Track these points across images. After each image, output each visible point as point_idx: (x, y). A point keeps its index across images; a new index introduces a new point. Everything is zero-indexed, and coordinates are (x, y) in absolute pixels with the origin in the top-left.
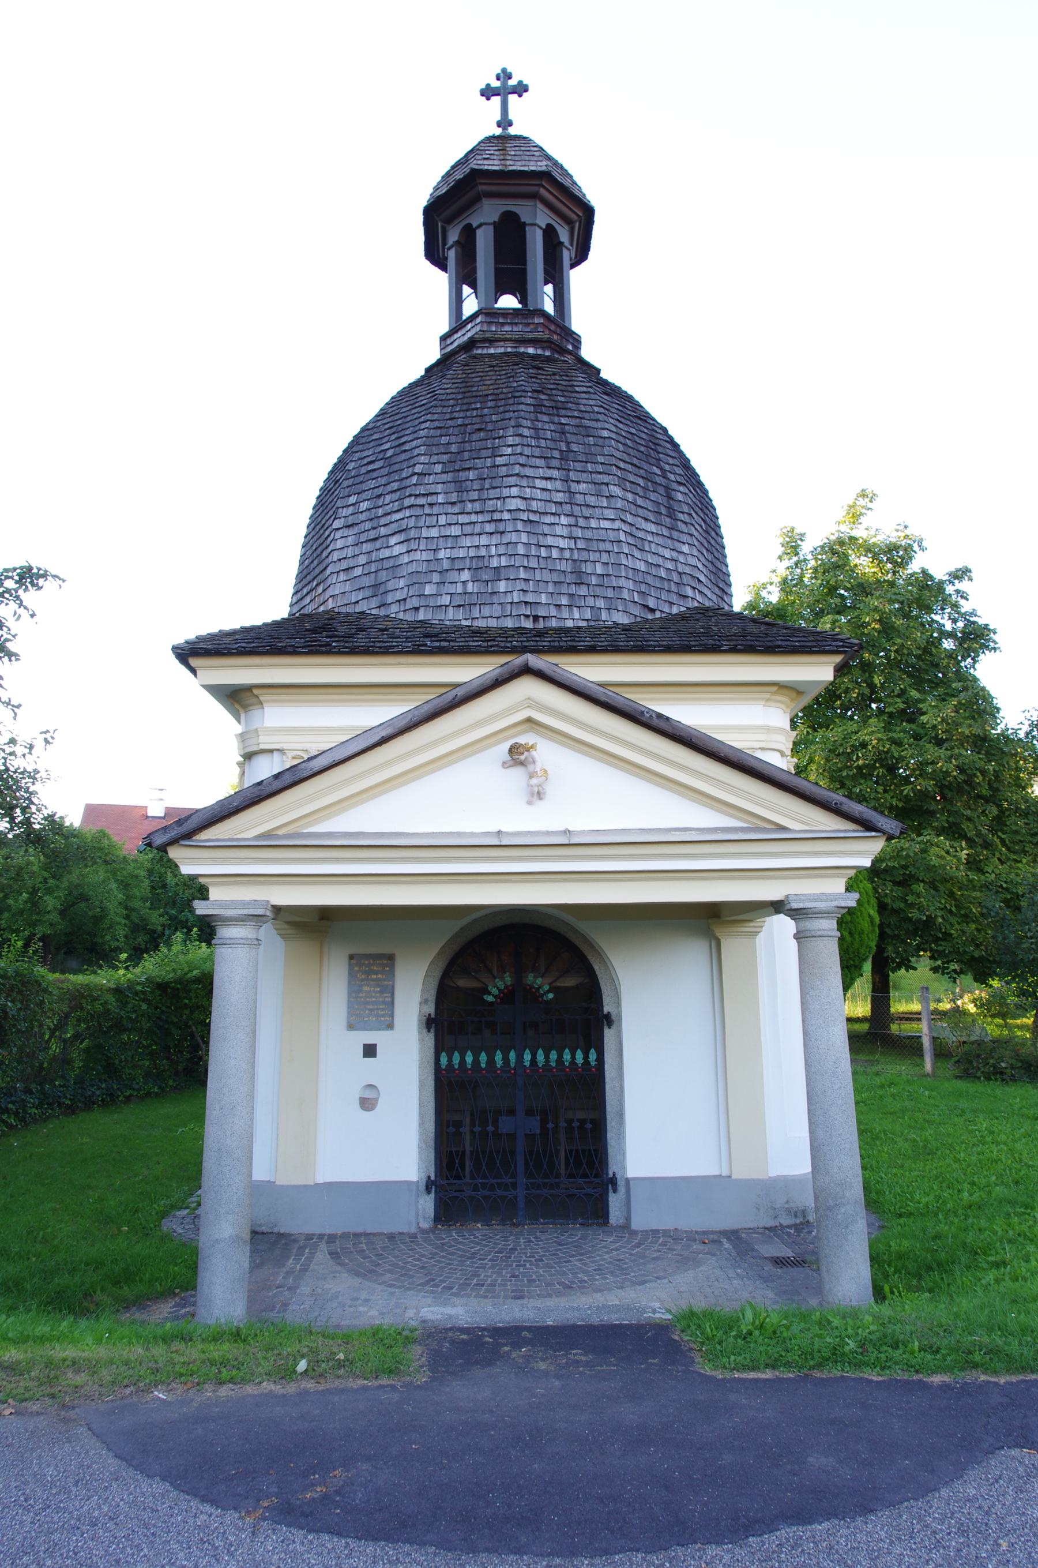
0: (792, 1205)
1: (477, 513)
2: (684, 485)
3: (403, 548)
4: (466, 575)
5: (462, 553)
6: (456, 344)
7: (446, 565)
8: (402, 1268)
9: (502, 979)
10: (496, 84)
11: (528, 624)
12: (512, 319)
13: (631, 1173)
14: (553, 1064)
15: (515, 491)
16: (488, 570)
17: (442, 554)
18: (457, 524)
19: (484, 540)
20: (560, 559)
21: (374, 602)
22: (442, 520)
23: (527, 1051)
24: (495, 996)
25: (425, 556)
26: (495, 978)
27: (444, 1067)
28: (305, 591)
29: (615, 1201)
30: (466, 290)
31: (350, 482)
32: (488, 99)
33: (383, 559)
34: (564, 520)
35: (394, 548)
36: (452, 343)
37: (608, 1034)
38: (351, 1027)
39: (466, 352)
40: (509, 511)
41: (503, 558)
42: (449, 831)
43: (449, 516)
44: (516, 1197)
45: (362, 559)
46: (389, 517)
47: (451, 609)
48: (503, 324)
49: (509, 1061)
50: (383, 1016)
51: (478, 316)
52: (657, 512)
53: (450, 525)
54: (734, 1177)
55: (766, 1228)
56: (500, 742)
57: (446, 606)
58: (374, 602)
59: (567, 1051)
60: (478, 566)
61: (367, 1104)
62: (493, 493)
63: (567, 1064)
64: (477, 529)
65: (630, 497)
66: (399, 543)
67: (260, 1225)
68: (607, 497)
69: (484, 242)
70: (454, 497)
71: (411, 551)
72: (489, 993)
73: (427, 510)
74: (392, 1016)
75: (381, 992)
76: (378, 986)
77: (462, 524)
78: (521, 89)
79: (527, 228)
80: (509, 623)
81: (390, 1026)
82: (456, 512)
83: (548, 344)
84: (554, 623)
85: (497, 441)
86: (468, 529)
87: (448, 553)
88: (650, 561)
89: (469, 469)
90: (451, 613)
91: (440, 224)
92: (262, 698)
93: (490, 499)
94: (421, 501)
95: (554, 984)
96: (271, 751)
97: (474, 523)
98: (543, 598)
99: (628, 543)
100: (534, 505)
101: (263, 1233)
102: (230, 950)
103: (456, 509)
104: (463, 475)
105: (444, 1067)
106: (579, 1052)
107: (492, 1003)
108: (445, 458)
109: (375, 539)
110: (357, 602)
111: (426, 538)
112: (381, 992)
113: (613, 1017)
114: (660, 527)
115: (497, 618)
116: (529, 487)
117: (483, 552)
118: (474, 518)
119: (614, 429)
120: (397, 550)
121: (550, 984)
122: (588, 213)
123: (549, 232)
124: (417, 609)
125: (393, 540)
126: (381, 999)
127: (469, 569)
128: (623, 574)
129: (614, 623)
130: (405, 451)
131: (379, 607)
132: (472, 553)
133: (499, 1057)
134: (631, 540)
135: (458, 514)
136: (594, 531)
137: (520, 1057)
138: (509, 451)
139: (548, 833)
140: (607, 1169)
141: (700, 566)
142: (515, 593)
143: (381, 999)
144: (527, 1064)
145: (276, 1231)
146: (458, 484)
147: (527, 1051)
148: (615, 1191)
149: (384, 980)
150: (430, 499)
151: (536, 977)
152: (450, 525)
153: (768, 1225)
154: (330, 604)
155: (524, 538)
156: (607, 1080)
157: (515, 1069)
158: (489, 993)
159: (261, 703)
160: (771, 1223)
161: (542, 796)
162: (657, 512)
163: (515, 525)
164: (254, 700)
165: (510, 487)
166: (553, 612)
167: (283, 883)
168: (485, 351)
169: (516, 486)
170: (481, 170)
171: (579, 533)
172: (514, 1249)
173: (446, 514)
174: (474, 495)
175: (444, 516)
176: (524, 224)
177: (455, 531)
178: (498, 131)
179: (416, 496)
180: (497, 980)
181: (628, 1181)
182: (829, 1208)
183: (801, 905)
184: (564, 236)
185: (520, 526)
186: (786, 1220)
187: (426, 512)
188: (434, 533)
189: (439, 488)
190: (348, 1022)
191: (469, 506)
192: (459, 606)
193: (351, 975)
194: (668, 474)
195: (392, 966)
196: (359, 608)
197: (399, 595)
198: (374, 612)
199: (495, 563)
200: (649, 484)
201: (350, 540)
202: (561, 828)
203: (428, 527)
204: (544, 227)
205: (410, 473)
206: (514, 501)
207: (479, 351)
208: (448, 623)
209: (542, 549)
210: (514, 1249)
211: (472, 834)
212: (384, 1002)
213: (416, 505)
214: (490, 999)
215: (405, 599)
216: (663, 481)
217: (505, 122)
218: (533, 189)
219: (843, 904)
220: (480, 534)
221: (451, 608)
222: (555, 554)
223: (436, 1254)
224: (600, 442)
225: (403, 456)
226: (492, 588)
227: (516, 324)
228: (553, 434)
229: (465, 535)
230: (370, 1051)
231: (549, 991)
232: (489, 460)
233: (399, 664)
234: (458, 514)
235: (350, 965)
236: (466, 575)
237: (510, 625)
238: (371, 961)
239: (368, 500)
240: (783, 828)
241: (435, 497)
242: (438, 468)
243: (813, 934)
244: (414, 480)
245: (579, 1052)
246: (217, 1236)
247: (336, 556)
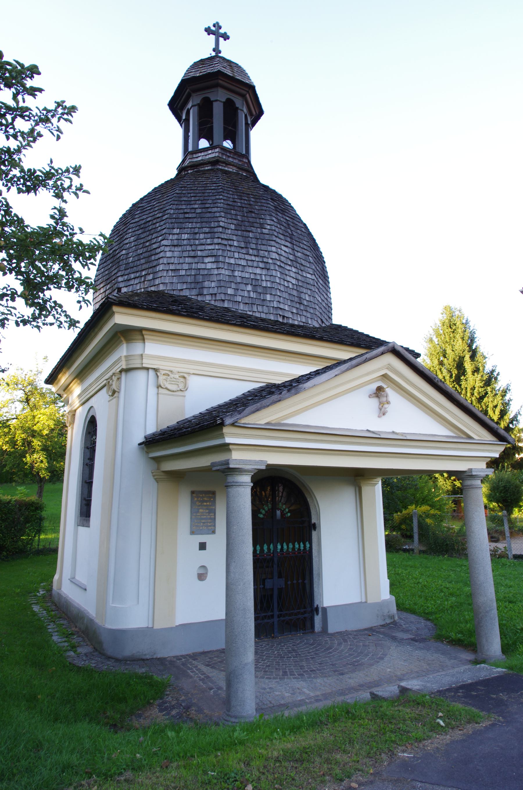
0: (390, 613)
1: (255, 256)
4: (249, 288)
5: (247, 275)
6: (200, 159)
7: (239, 280)
10: (213, 29)
11: (280, 320)
13: (325, 605)
14: (290, 550)
15: (274, 249)
16: (261, 287)
17: (236, 274)
18: (244, 259)
19: (258, 271)
21: (194, 292)
23: (279, 544)
24: (264, 515)
25: (227, 272)
29: (318, 620)
32: (209, 34)
33: (200, 269)
34: (294, 270)
35: (208, 264)
36: (197, 157)
37: (314, 533)
38: (192, 533)
39: (212, 166)
40: (272, 259)
43: (240, 254)
44: (273, 622)
45: (186, 267)
46: (204, 246)
47: (241, 304)
48: (229, 157)
49: (270, 550)
50: (210, 526)
51: (217, 148)
53: (241, 259)
54: (369, 602)
55: (381, 626)
57: (239, 302)
58: (194, 292)
59: (296, 543)
60: (255, 283)
61: (202, 577)
62: (263, 248)
63: (296, 550)
64: (255, 264)
66: (211, 262)
67: (145, 655)
69: (218, 110)
70: (242, 244)
71: (220, 268)
72: (261, 513)
74: (215, 526)
75: (209, 513)
76: (207, 509)
77: (247, 260)
78: (226, 37)
80: (272, 318)
81: (214, 532)
82: (244, 252)
84: (291, 321)
86: (250, 263)
87: (240, 274)
89: (249, 231)
90: (242, 307)
91: (188, 90)
92: (145, 337)
93: (262, 250)
94: (225, 242)
95: (290, 509)
96: (147, 369)
97: (254, 261)
98: (286, 308)
100: (283, 259)
101: (147, 660)
102: (243, 489)
103: (244, 251)
106: (301, 543)
107: (262, 519)
109: (194, 257)
110: (182, 290)
111: (228, 263)
112: (209, 513)
113: (317, 526)
115: (266, 313)
117: (258, 277)
118: (253, 258)
120: (209, 266)
122: (261, 113)
124: (223, 301)
125: (207, 260)
126: (209, 517)
127: (251, 285)
129: (314, 326)
130: (210, 212)
131: (197, 295)
132: (252, 276)
133: (265, 547)
135: (245, 254)
137: (275, 547)
138: (269, 227)
140: (314, 603)
142: (275, 302)
143: (209, 517)
144: (279, 550)
145: (155, 657)
147: (279, 544)
148: (317, 614)
150: (230, 242)
152: (241, 259)
153: (381, 624)
154: (162, 288)
155: (279, 275)
156: (314, 558)
159: (144, 340)
160: (383, 623)
163: (275, 267)
164: (140, 337)
166: (290, 315)
167: (438, 459)
168: (223, 168)
169: (274, 246)
170: (223, 73)
173: (239, 252)
174: (254, 246)
175: (237, 253)
177: (243, 263)
178: (214, 54)
179: (222, 239)
181: (325, 610)
182: (487, 612)
183: (237, 466)
185: (277, 268)
186: (388, 621)
188: (232, 261)
191: (251, 251)
192: (246, 303)
193: (193, 503)
195: (214, 498)
196: (183, 293)
197: (211, 291)
198: (193, 297)
199: (264, 284)
201: (176, 254)
202: (390, 431)
203: (229, 257)
206: (274, 254)
207: (220, 167)
208: (240, 311)
209: (286, 282)
211: (356, 430)
212: (210, 519)
213: (222, 244)
214: (261, 516)
215: (216, 294)
217: (217, 50)
218: (244, 92)
220: (257, 267)
221: (242, 304)
222: (291, 286)
225: (208, 215)
226: (263, 297)
227: (235, 159)
229: (249, 266)
230: (203, 546)
231: (288, 512)
233: (229, 330)
234: (245, 254)
235: (192, 496)
236: (249, 288)
237: (272, 319)
238: (204, 495)
239: (188, 234)
240: (470, 437)
241: (232, 242)
243: (477, 486)
245: (301, 543)
246: (246, 661)
247: (165, 261)
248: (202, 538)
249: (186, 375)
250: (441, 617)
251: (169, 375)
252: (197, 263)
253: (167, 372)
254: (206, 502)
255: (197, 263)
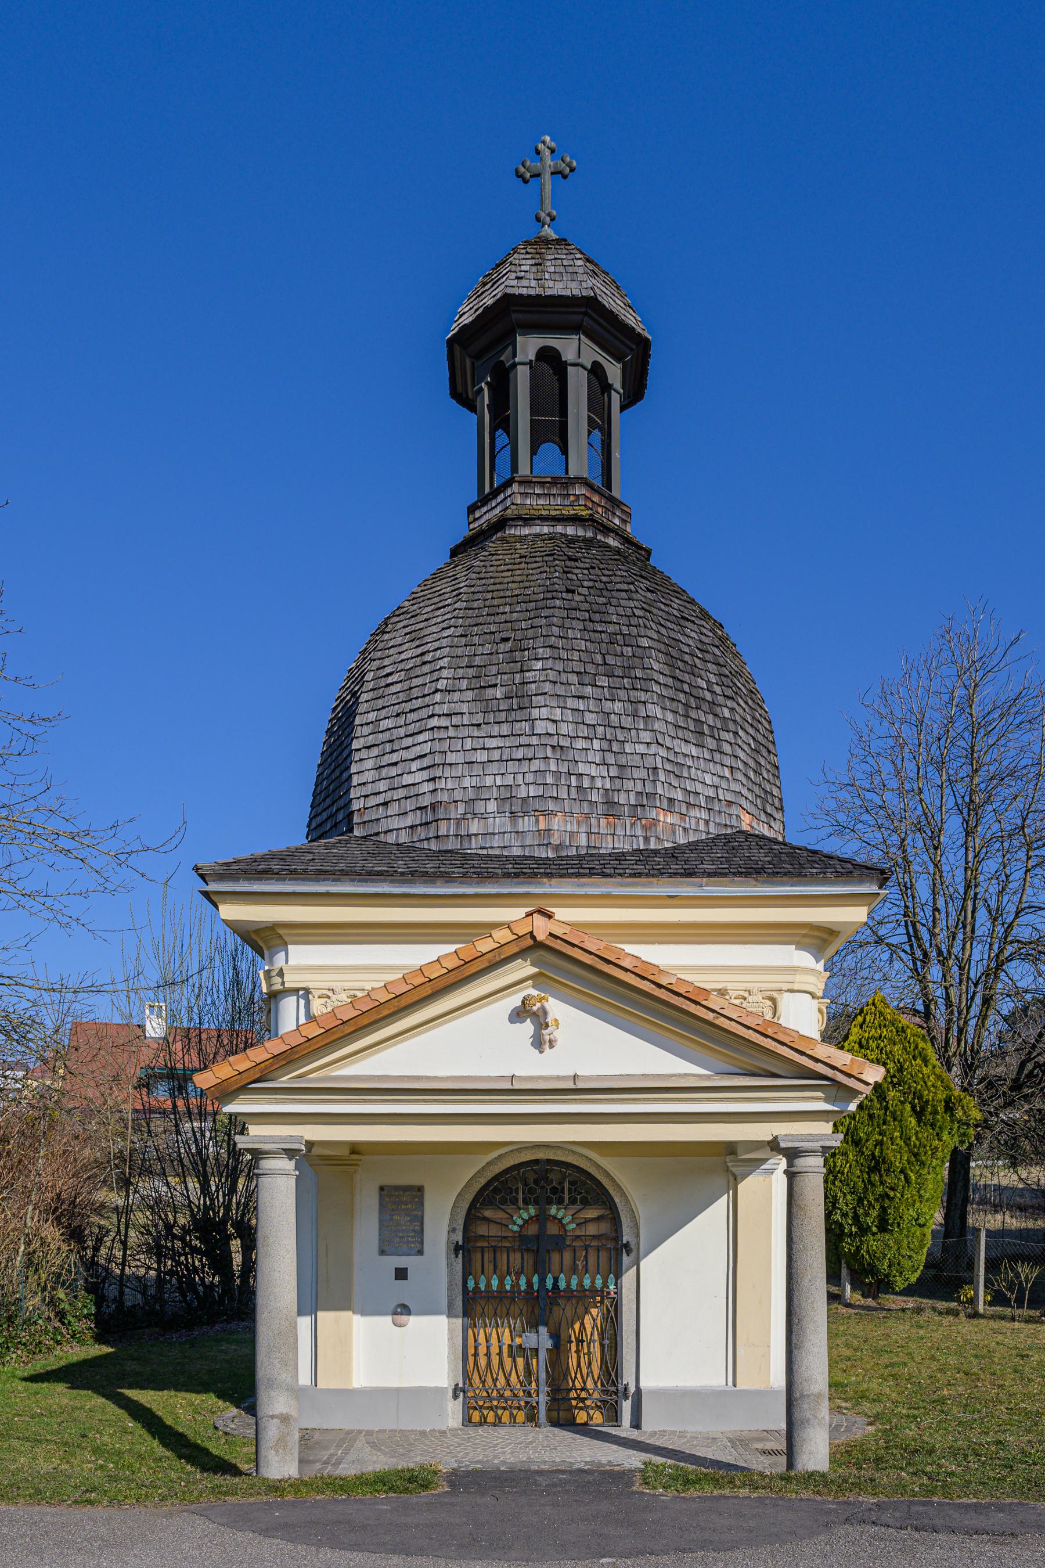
2: (732, 698)
3: (425, 775)
8: (432, 1453)
9: (527, 1210)
12: (549, 488)
20: (591, 788)
22: (469, 744)
26: (520, 1209)
27: (471, 1289)
28: (325, 815)
30: (500, 432)
31: (370, 695)
41: (531, 787)
42: (466, 1074)
50: (413, 1242)
52: (699, 733)
56: (514, 993)
65: (670, 717)
68: (644, 717)
70: (479, 719)
72: (514, 1223)
73: (452, 732)
79: (569, 368)
83: (590, 523)
85: (526, 653)
88: (688, 788)
99: (665, 770)
104: (490, 693)
105: (471, 1289)
108: (471, 672)
112: (411, 1221)
114: (701, 749)
116: (559, 707)
119: (655, 636)
121: (572, 1215)
123: (596, 371)
128: (658, 805)
134: (668, 767)
136: (629, 757)
139: (559, 1078)
141: (745, 792)
146: (484, 703)
149: (414, 1210)
150: (456, 720)
151: (558, 1209)
157: (538, 1291)
158: (514, 1223)
161: (554, 1044)
162: (699, 733)
165: (539, 707)
171: (610, 759)
172: (531, 1442)
176: (565, 364)
177: (482, 756)
180: (522, 1211)
183: (790, 1145)
184: (614, 372)
187: (450, 735)
189: (464, 708)
190: (380, 1248)
194: (715, 686)
199: (522, 793)
200: (692, 700)
204: (589, 367)
205: (433, 690)
210: (531, 1442)
216: (708, 696)
219: (828, 1144)
223: (463, 1444)
224: (639, 652)
225: (426, 669)
228: (588, 644)
232: (518, 675)
238: (401, 1193)
242: (464, 684)
244: (438, 697)
248: (402, 1262)
249: (775, 995)
250: (915, 1417)
251: (329, 997)
252: (402, 774)
253: (326, 992)
254: (406, 1203)
255: (402, 774)
